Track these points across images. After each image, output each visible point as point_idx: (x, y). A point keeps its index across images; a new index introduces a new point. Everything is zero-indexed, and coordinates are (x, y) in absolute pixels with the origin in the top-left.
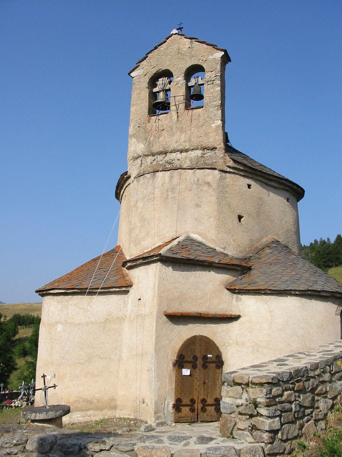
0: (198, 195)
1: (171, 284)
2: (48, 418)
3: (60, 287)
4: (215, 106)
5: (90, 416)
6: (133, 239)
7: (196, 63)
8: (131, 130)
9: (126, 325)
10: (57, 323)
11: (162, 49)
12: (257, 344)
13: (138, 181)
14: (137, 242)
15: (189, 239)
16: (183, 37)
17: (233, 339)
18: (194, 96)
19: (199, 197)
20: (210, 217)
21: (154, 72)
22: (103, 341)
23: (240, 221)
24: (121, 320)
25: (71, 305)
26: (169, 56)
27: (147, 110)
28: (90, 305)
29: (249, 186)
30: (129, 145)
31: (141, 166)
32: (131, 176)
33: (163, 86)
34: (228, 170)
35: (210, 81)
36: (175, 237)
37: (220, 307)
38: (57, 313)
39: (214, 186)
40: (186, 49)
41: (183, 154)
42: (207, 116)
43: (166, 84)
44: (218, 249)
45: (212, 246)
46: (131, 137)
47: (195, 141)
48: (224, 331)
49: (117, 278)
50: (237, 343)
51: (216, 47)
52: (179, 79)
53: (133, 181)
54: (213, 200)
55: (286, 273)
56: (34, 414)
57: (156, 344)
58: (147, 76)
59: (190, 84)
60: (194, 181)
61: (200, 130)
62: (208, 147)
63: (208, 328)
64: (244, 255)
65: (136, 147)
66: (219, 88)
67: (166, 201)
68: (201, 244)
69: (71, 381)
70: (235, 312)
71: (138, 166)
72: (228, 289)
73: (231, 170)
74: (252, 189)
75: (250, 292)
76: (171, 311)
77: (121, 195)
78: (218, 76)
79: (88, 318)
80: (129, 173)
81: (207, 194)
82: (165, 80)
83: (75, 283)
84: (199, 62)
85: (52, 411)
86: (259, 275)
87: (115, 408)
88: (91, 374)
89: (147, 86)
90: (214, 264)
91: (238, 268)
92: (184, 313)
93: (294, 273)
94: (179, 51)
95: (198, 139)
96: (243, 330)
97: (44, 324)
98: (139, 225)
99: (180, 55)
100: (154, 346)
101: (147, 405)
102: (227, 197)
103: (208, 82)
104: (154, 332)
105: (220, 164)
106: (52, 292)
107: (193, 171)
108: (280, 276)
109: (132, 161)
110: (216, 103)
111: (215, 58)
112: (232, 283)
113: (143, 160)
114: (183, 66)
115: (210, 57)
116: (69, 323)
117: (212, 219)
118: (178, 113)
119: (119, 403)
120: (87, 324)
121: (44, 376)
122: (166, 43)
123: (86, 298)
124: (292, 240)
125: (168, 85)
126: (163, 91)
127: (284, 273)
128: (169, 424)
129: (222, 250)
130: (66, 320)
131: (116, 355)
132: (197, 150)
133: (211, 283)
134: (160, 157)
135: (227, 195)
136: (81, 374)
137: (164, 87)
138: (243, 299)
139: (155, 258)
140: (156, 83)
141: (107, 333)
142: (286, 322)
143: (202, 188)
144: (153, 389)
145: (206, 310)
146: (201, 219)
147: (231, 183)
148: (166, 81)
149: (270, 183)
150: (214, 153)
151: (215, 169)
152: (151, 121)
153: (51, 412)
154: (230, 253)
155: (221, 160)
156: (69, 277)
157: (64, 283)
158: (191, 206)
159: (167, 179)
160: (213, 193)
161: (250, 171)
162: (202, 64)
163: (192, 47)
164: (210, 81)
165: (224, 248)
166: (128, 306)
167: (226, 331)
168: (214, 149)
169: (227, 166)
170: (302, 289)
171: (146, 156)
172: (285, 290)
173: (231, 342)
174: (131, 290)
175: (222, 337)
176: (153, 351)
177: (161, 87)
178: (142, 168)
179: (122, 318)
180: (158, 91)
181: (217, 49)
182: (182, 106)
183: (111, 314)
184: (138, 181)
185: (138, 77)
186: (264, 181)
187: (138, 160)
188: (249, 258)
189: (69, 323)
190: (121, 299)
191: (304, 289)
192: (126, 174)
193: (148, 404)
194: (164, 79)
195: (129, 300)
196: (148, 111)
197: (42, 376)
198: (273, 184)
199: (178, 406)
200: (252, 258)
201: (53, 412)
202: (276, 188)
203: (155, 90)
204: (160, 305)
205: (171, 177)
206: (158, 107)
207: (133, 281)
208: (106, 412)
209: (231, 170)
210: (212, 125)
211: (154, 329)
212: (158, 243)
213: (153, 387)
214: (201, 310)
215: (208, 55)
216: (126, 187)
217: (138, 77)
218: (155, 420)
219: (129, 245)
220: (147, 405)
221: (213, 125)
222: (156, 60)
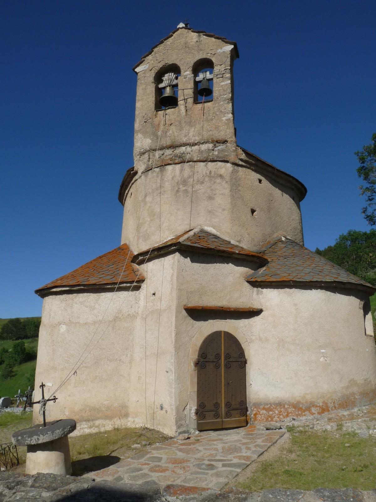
1: (190, 276)
2: (55, 438)
3: (64, 284)
4: (225, 99)
5: (98, 427)
6: (141, 234)
7: (204, 57)
8: (137, 126)
9: (138, 323)
10: (60, 324)
11: (169, 43)
12: (283, 340)
13: (146, 176)
14: (147, 237)
15: (202, 231)
16: (190, 31)
17: (255, 334)
18: (203, 92)
19: (212, 190)
20: (224, 210)
21: (161, 67)
22: (113, 342)
23: (253, 215)
24: (133, 317)
25: (76, 303)
26: (176, 50)
27: (154, 104)
28: (97, 303)
29: (260, 181)
30: (135, 141)
31: (149, 161)
32: (139, 172)
33: (169, 81)
34: (241, 163)
35: (220, 74)
36: (188, 230)
37: (241, 300)
38: (60, 312)
39: (228, 178)
40: (194, 43)
42: (217, 109)
43: (173, 79)
44: (233, 242)
45: (227, 239)
46: (139, 131)
47: (206, 135)
48: (246, 326)
49: (128, 273)
50: (260, 339)
51: (225, 40)
52: (187, 73)
53: (141, 177)
54: (227, 193)
55: (306, 266)
56: (35, 437)
57: (176, 341)
58: (153, 71)
59: (198, 79)
60: (206, 173)
61: (210, 124)
62: (220, 140)
63: (229, 323)
64: (258, 249)
65: (141, 142)
66: (229, 82)
68: (216, 237)
69: (76, 387)
70: (256, 306)
71: (146, 160)
72: (248, 282)
73: (243, 164)
74: (263, 184)
75: (273, 284)
76: (191, 305)
77: (125, 194)
78: (227, 69)
79: (95, 317)
80: (135, 169)
81: (220, 187)
82: (172, 75)
83: (81, 280)
84: (208, 55)
85: (59, 429)
86: (278, 267)
88: (100, 378)
89: (153, 81)
90: (234, 255)
91: (253, 260)
92: (205, 307)
93: (314, 265)
94: (186, 45)
95: (208, 133)
96: (266, 325)
97: (45, 326)
98: (149, 220)
99: (187, 49)
100: (174, 343)
101: (166, 411)
102: (239, 190)
103: (217, 75)
104: (173, 329)
105: (233, 158)
106: (55, 290)
108: (302, 268)
109: (139, 156)
110: (226, 96)
111: (224, 52)
112: (252, 275)
113: (151, 154)
114: (190, 60)
115: (219, 50)
117: (226, 212)
118: (186, 107)
119: (131, 410)
120: (94, 323)
121: (42, 386)
122: (172, 37)
123: (91, 297)
124: (298, 238)
125: (175, 80)
126: (170, 86)
127: (305, 266)
128: (192, 433)
129: (237, 244)
130: (71, 319)
132: (208, 144)
133: (230, 275)
134: (168, 152)
135: (240, 188)
136: (88, 379)
137: (171, 82)
139: (173, 248)
140: (162, 78)
141: (117, 332)
142: (312, 315)
143: (215, 181)
144: (174, 393)
145: (227, 304)
146: (214, 212)
147: (243, 176)
148: (172, 76)
150: (226, 146)
151: (227, 162)
152: (158, 116)
153: (58, 431)
154: (245, 247)
155: (232, 153)
156: (73, 275)
157: (68, 280)
158: (204, 199)
159: (178, 172)
160: (226, 186)
162: (210, 58)
163: (200, 41)
164: (220, 74)
165: (239, 242)
166: (140, 303)
167: (247, 326)
168: (225, 142)
169: (239, 159)
170: (328, 281)
171: (153, 150)
172: (311, 281)
173: (253, 338)
174: (144, 285)
175: (244, 333)
176: (172, 350)
177: (168, 82)
178: (150, 163)
179: (134, 316)
180: (164, 86)
181: (227, 43)
182: (190, 101)
183: (121, 311)
184: (146, 176)
185: (144, 72)
187: (145, 155)
188: (264, 252)
190: (132, 295)
191: (330, 281)
192: (133, 170)
193: (168, 410)
194: (170, 74)
195: (141, 295)
196: (154, 106)
197: (41, 386)
200: (266, 252)
201: (61, 430)
203: (161, 86)
204: (179, 298)
205: (182, 170)
206: (165, 102)
207: (145, 276)
209: (243, 164)
211: (174, 325)
212: (170, 237)
213: (173, 390)
214: (221, 303)
215: (217, 49)
216: (132, 184)
217: (144, 72)
218: (176, 429)
219: (138, 240)
220: (166, 411)
221: (224, 119)
222: (162, 55)
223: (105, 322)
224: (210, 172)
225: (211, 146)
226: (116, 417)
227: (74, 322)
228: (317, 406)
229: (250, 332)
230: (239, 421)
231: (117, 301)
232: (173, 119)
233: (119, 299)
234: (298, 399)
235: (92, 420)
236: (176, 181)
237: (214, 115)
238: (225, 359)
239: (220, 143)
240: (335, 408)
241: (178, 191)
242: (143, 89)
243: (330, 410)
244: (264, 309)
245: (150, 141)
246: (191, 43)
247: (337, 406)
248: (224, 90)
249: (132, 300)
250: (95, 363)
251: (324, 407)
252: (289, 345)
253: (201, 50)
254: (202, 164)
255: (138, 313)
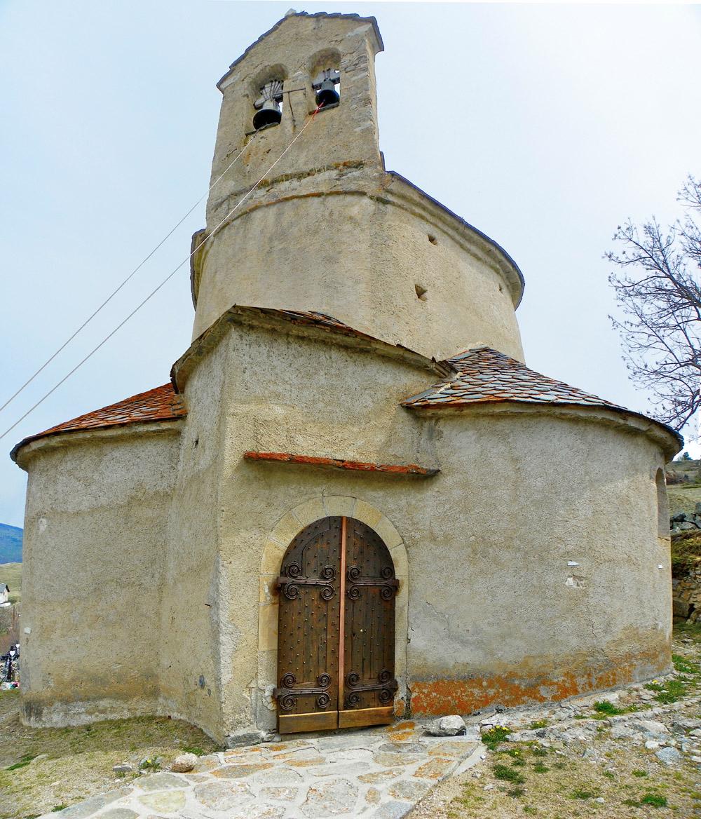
0: (332, 239)
41: (304, 181)
42: (346, 117)
48: (401, 510)
50: (434, 539)
53: (212, 243)
67: (269, 259)
70: (426, 464)
75: (466, 411)
87: (154, 693)
96: (447, 506)
107: (321, 199)
116: (58, 513)
131: (153, 577)
138: (445, 433)
145: (357, 457)
146: (338, 286)
149: (468, 245)
161: (430, 207)
179: (166, 494)
184: (220, 239)
186: (458, 237)
189: (58, 513)
198: (473, 248)
199: (281, 702)
202: (479, 259)
205: (279, 215)
208: (137, 701)
210: (355, 130)
215: (346, 33)
221: (358, 130)
223: (112, 508)
224: (331, 214)
225: (334, 173)
226: (135, 696)
227: (59, 510)
228: (552, 684)
229: (410, 522)
230: (378, 714)
231: (133, 465)
232: (273, 143)
233: (138, 460)
234: (511, 668)
235: (94, 699)
236: (268, 235)
237: (341, 126)
238: (347, 581)
239: (350, 167)
240: (591, 685)
241: (269, 252)
242: (229, 109)
243: (580, 690)
244: (445, 471)
245: (234, 183)
246: (306, 33)
247: (595, 682)
248: (358, 88)
249: (163, 462)
250: (95, 590)
251: (567, 685)
252: (497, 550)
253: (320, 39)
254: (316, 200)
255: (174, 489)
